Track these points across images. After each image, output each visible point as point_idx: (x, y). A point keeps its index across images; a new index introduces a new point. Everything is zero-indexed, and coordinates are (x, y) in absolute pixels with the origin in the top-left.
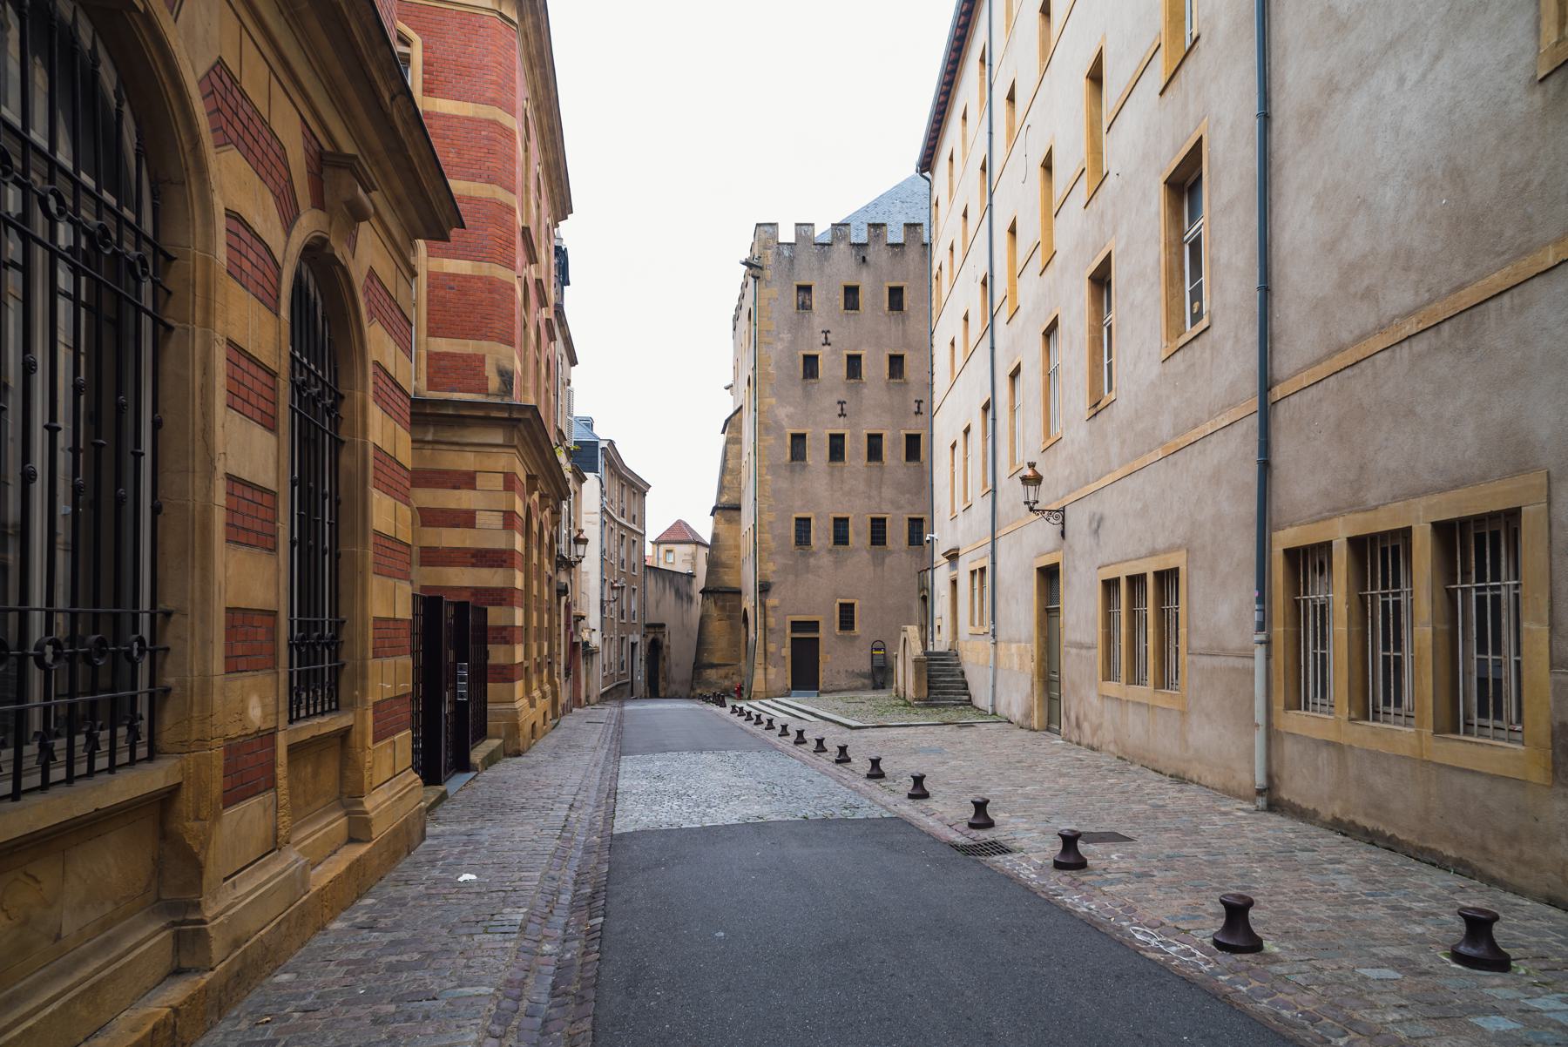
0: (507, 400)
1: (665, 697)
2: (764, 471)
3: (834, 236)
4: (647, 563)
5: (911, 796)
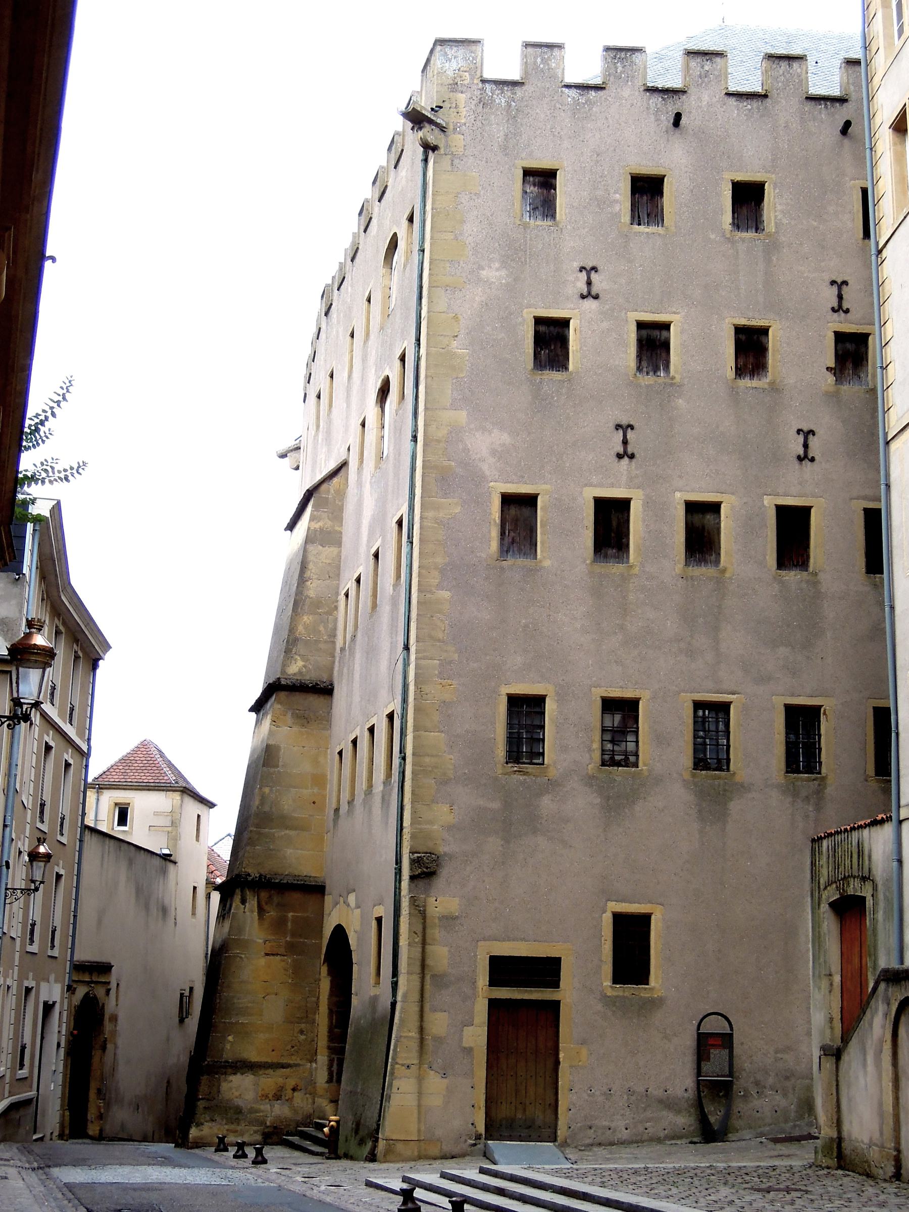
2: (434, 579)
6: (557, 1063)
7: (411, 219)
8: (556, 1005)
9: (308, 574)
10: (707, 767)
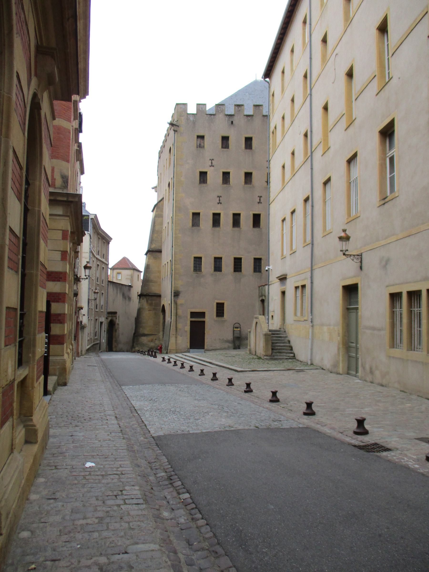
0: (65, 191)
1: (116, 351)
3: (217, 111)
4: (109, 280)
5: (305, 414)
7: (173, 145)
8: (204, 322)
9: (155, 225)
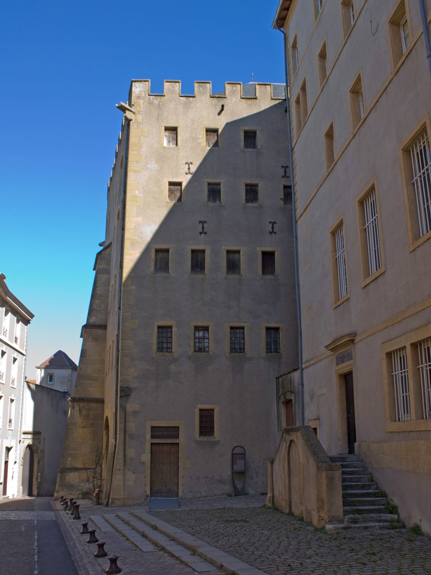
6: (178, 467)
10: (236, 352)
